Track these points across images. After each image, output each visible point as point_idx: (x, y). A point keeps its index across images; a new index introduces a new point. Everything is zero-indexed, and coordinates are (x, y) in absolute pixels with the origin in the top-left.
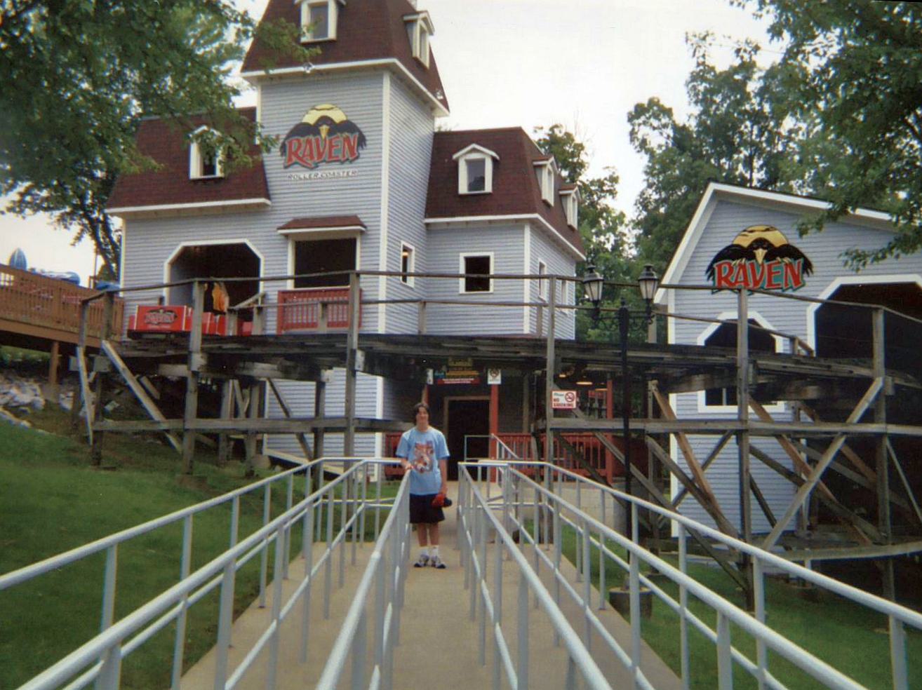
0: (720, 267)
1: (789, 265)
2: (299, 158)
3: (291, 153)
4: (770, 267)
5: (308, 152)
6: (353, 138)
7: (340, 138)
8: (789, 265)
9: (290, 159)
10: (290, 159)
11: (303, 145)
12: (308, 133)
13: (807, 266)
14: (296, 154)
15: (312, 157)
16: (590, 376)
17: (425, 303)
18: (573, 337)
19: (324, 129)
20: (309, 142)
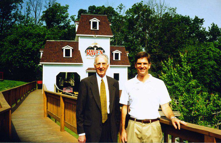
0: (87, 51)
1: (101, 51)
2: (89, 54)
3: (88, 53)
4: (97, 51)
5: (92, 53)
6: (102, 51)
7: (99, 51)
8: (101, 51)
9: (87, 54)
10: (87, 54)
11: (91, 52)
12: (92, 49)
13: (104, 51)
14: (89, 53)
15: (93, 54)
16: (29, 55)
17: (161, 110)
18: (120, 90)
19: (95, 49)
20: (92, 51)
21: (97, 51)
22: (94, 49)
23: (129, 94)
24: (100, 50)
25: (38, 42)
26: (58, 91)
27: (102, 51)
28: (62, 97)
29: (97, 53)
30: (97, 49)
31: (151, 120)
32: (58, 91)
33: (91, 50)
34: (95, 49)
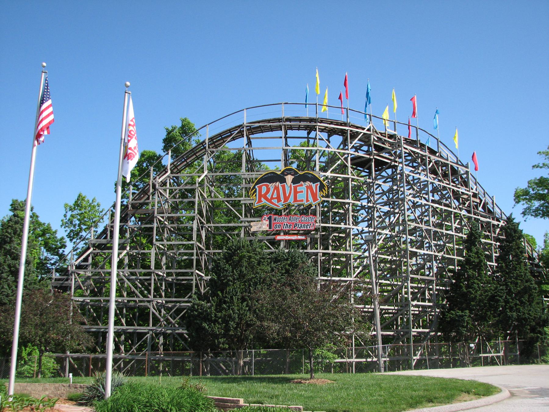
0: (260, 188)
3: (260, 196)
4: (295, 188)
5: (275, 196)
19: (289, 178)
20: (277, 188)
21: (295, 188)
22: (283, 181)
23: (513, 208)
24: (308, 183)
25: (36, 237)
26: (147, 201)
27: (314, 186)
28: (124, 326)
29: (296, 192)
30: (294, 181)
31: (450, 368)
32: (147, 201)
33: (272, 186)
34: (289, 178)
